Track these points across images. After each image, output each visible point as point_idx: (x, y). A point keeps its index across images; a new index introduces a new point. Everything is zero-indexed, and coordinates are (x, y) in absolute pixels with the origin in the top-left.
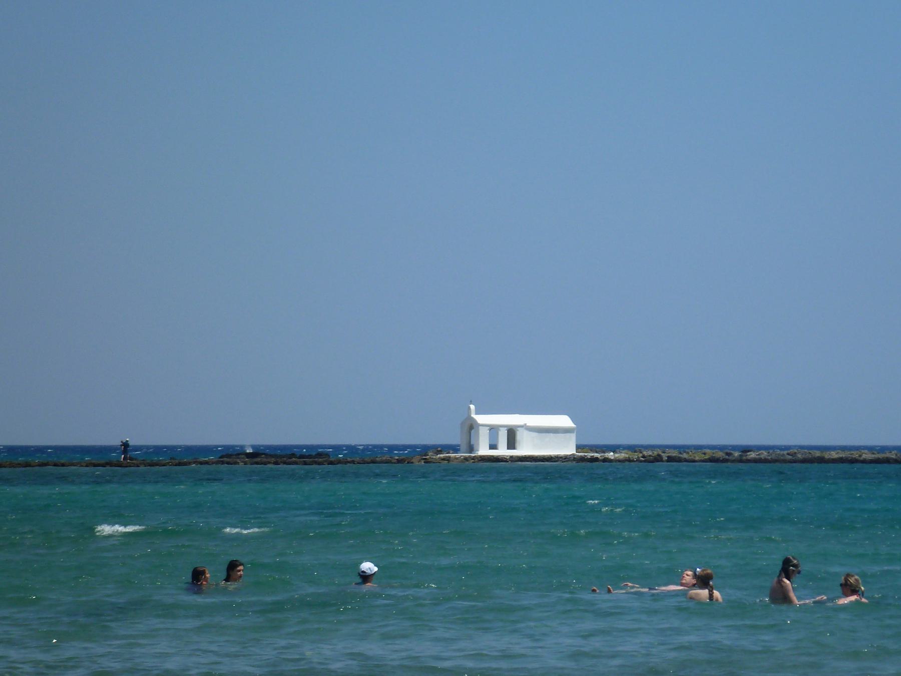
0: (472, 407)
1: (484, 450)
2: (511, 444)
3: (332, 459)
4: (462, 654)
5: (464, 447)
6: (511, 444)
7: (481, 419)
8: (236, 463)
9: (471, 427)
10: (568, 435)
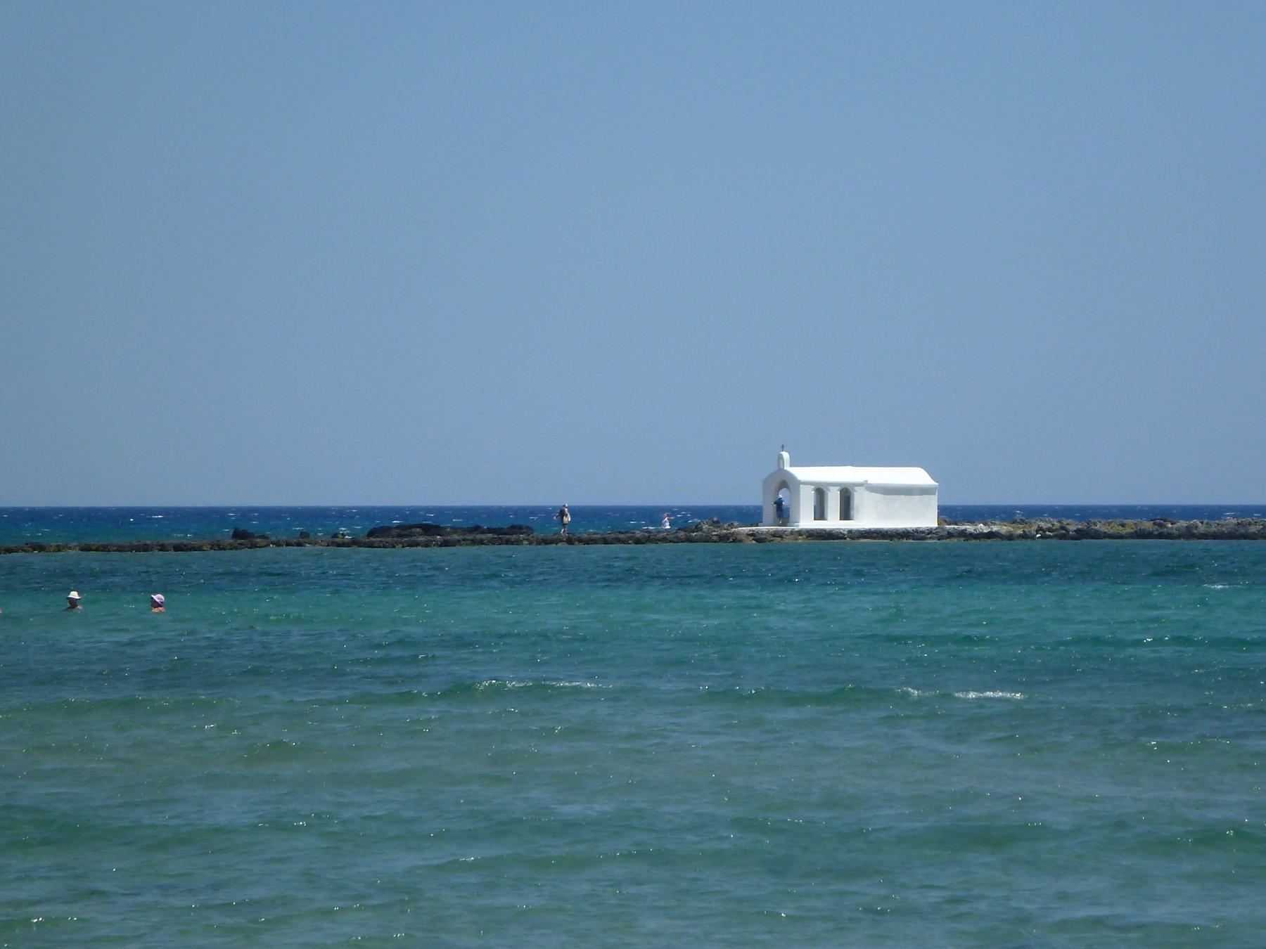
0: (785, 455)
1: (806, 521)
2: (846, 514)
3: (638, 534)
4: (394, 690)
5: (769, 512)
6: (846, 514)
7: (803, 473)
8: (518, 542)
9: (786, 482)
10: (926, 497)
